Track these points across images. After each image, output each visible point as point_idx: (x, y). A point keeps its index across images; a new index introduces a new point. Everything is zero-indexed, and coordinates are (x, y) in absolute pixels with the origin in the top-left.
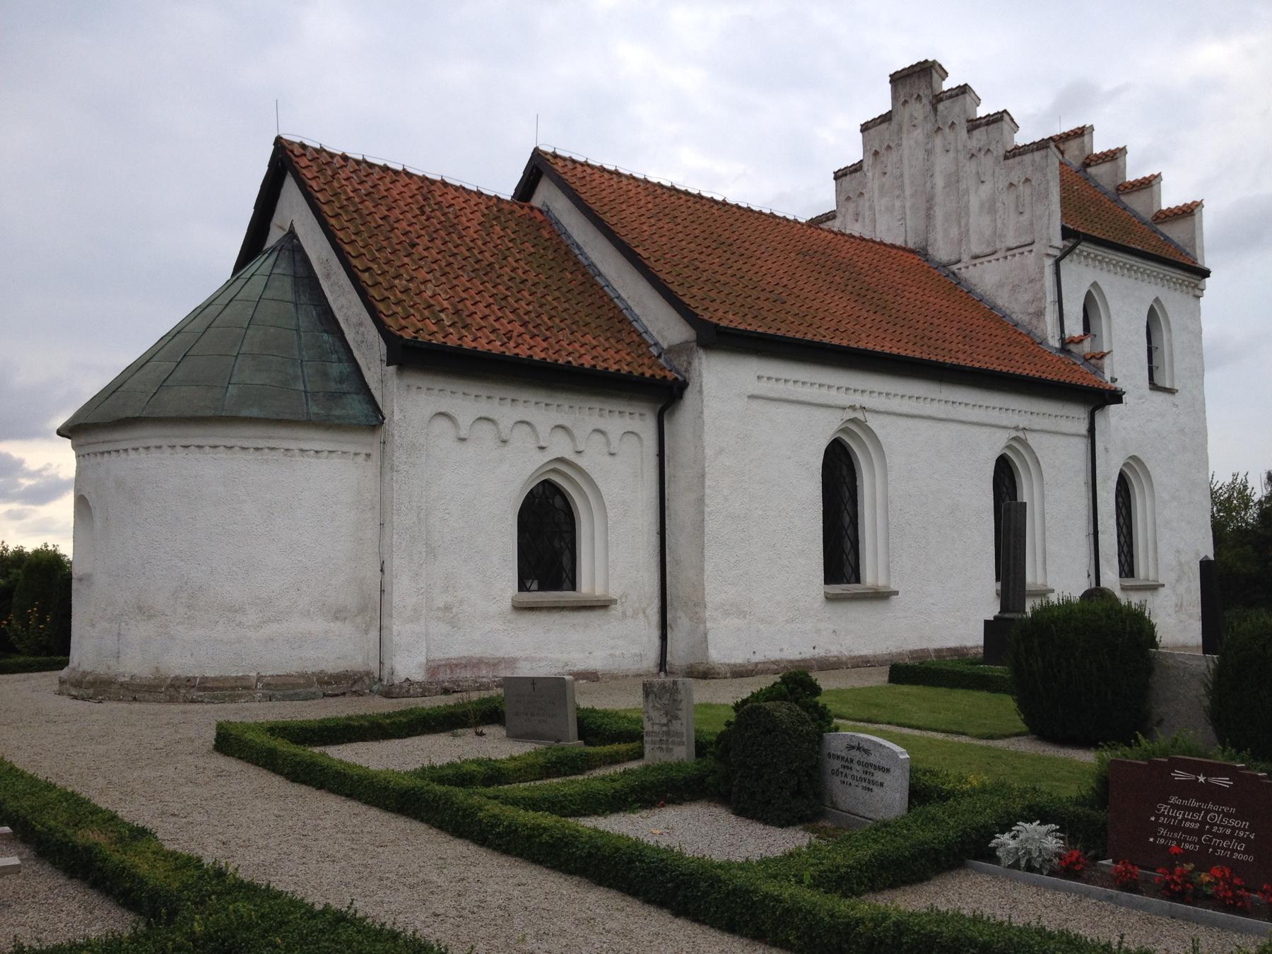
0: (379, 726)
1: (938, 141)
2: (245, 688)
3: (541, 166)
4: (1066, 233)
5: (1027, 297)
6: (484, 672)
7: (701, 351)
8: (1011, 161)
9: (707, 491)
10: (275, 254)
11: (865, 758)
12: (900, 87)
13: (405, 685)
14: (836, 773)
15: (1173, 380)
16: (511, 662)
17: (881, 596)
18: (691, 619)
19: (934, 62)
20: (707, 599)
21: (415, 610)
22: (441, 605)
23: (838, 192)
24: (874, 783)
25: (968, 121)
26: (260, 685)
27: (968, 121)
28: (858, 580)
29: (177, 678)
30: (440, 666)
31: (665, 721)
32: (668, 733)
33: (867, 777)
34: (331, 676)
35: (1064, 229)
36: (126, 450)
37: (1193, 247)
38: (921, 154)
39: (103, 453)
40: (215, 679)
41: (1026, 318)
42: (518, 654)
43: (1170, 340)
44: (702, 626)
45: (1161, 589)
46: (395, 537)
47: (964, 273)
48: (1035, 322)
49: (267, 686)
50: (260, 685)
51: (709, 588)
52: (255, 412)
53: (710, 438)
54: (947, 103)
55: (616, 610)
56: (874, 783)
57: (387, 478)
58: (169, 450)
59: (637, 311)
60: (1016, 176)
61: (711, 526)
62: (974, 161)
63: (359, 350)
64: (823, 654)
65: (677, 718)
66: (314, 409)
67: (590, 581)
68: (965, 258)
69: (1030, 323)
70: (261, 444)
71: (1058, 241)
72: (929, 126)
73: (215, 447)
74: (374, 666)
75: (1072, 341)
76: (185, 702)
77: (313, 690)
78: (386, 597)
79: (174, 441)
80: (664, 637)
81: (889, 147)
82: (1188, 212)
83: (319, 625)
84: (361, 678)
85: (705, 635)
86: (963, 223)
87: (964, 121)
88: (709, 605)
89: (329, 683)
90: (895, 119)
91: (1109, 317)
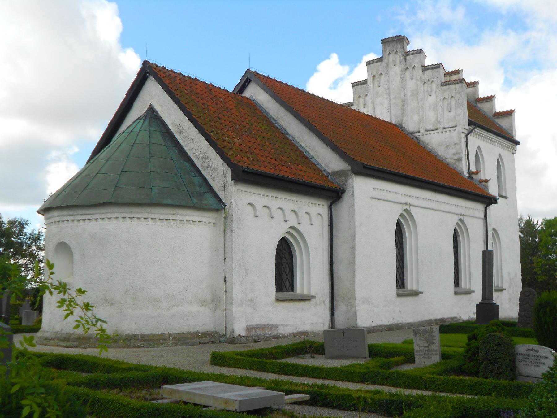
0: (272, 354)
1: (408, 74)
2: (164, 340)
3: (250, 77)
4: (470, 123)
5: (454, 151)
6: (267, 332)
7: (353, 176)
8: (444, 87)
9: (357, 243)
10: (142, 120)
11: (536, 354)
12: (387, 46)
13: (239, 337)
14: (521, 361)
15: (506, 191)
16: (276, 327)
17: (416, 294)
18: (347, 306)
19: (404, 36)
20: (357, 295)
21: (241, 301)
22: (250, 298)
23: (354, 94)
24: (540, 363)
25: (422, 66)
26: (171, 338)
27: (422, 66)
28: (292, 290)
29: (128, 335)
30: (251, 328)
31: (426, 345)
32: (429, 350)
33: (537, 361)
34: (201, 334)
35: (469, 120)
36: (96, 219)
37: (512, 131)
38: (398, 79)
39: (79, 220)
40: (148, 335)
41: (453, 161)
42: (278, 323)
43: (504, 174)
44: (353, 309)
45: (504, 291)
46: (234, 264)
47: (422, 138)
48: (457, 163)
49: (174, 338)
50: (171, 338)
51: (357, 290)
52: (169, 201)
53: (358, 219)
54: (412, 56)
55: (313, 301)
56: (540, 363)
57: (228, 235)
58: (122, 220)
59: (312, 153)
60: (446, 95)
61: (358, 260)
63: (205, 170)
64: (396, 322)
65: (433, 343)
66: (195, 200)
67: (301, 287)
68: (422, 131)
69: (455, 164)
70: (169, 217)
71: (467, 127)
72: (403, 66)
73: (117, 218)
74: (221, 329)
75: (473, 173)
76: (134, 347)
77: (195, 340)
78: (227, 294)
81: (381, 74)
82: (509, 114)
83: (195, 308)
84: (214, 335)
85: (356, 313)
86: (421, 114)
87: (420, 66)
88: (357, 299)
89: (201, 337)
90: (385, 61)
91: (484, 162)
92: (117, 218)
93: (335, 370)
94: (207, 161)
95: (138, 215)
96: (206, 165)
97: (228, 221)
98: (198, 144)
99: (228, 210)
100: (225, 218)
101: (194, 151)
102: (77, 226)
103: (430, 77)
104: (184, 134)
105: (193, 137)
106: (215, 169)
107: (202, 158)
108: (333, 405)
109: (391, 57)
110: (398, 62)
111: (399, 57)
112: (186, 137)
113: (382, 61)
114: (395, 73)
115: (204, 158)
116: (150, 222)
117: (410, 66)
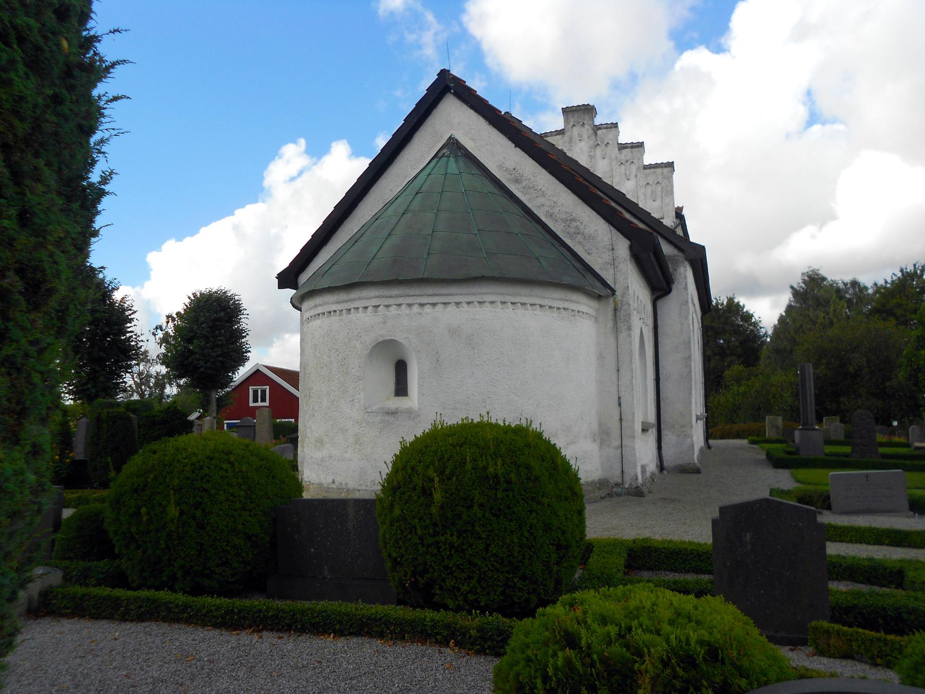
1: (599, 151)
12: (570, 116)
36: (458, 304)
44: (689, 440)
54: (604, 131)
57: (622, 336)
58: (500, 306)
62: (622, 166)
72: (592, 142)
79: (410, 300)
80: (659, 448)
87: (615, 144)
90: (568, 134)
92: (492, 303)
93: (871, 530)
94: (574, 224)
95: (523, 300)
96: (572, 230)
97: (622, 314)
98: (555, 199)
99: (619, 298)
100: (615, 310)
101: (546, 209)
102: (420, 314)
103: (628, 158)
104: (524, 184)
105: (544, 189)
106: (591, 237)
107: (564, 220)
108: (684, 568)
109: (576, 130)
110: (585, 136)
111: (586, 131)
112: (529, 188)
113: (564, 134)
114: (581, 150)
115: (567, 220)
116: (538, 311)
117: (602, 142)
